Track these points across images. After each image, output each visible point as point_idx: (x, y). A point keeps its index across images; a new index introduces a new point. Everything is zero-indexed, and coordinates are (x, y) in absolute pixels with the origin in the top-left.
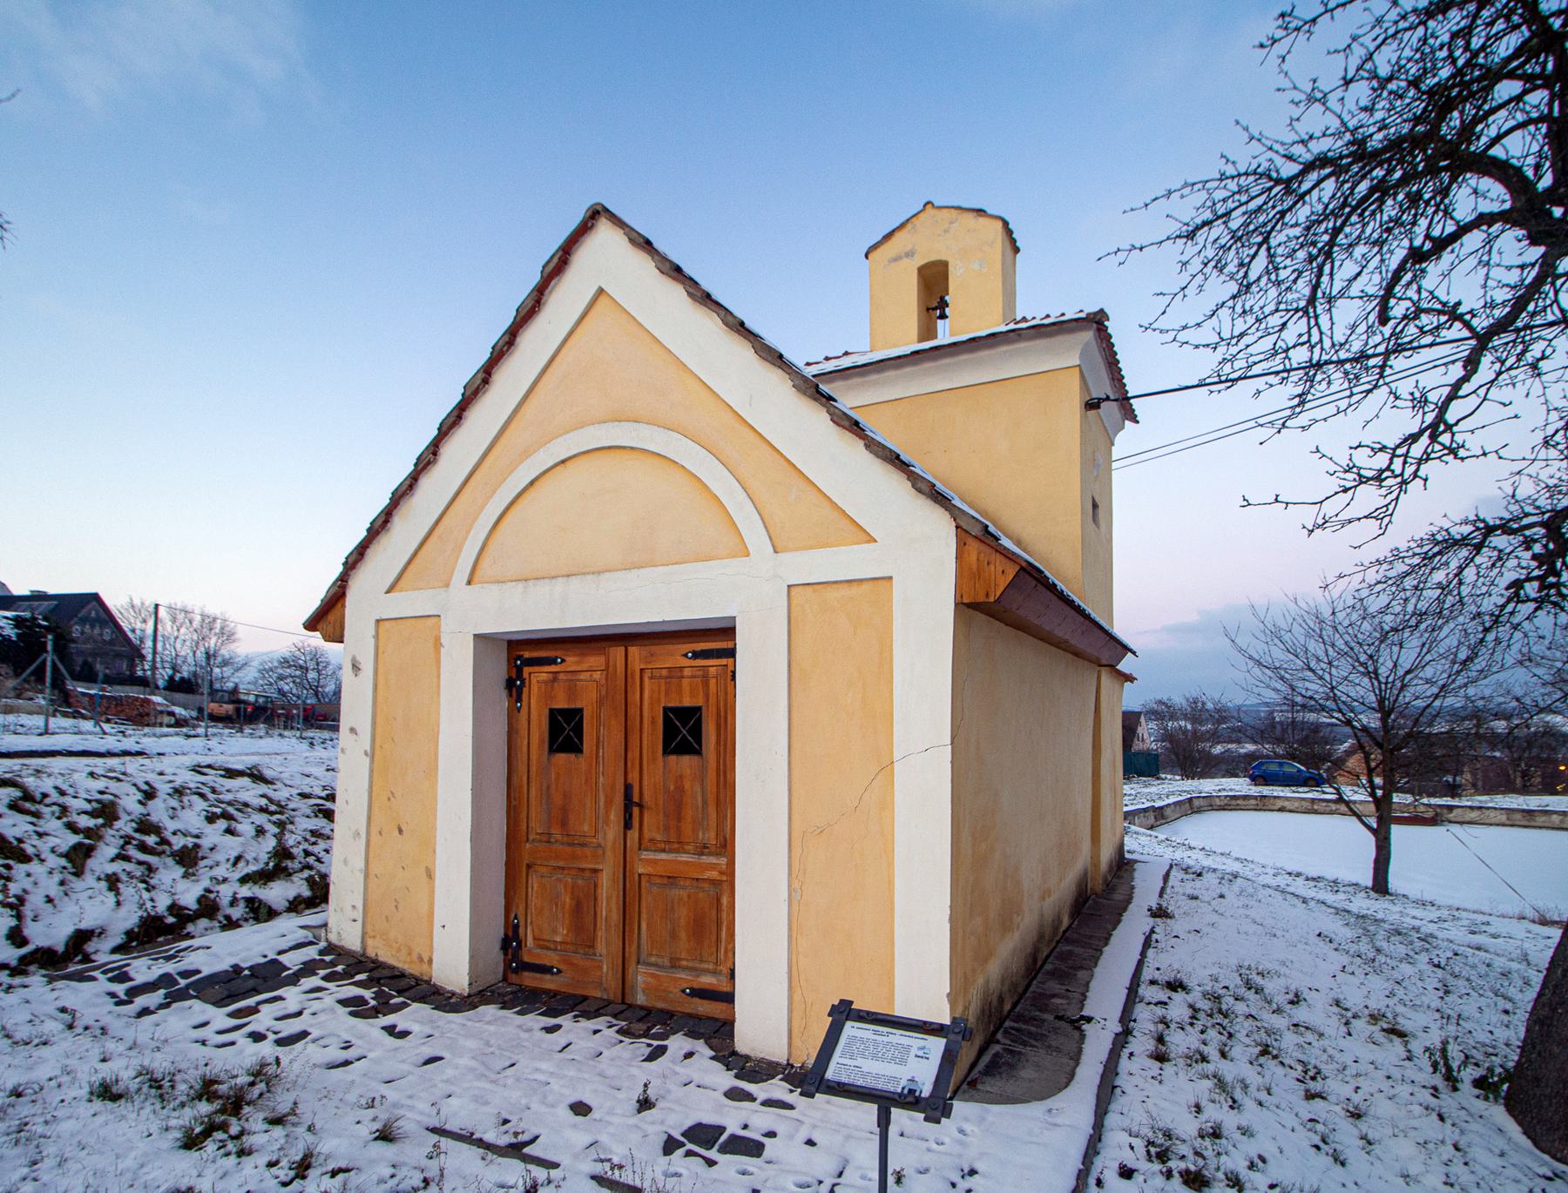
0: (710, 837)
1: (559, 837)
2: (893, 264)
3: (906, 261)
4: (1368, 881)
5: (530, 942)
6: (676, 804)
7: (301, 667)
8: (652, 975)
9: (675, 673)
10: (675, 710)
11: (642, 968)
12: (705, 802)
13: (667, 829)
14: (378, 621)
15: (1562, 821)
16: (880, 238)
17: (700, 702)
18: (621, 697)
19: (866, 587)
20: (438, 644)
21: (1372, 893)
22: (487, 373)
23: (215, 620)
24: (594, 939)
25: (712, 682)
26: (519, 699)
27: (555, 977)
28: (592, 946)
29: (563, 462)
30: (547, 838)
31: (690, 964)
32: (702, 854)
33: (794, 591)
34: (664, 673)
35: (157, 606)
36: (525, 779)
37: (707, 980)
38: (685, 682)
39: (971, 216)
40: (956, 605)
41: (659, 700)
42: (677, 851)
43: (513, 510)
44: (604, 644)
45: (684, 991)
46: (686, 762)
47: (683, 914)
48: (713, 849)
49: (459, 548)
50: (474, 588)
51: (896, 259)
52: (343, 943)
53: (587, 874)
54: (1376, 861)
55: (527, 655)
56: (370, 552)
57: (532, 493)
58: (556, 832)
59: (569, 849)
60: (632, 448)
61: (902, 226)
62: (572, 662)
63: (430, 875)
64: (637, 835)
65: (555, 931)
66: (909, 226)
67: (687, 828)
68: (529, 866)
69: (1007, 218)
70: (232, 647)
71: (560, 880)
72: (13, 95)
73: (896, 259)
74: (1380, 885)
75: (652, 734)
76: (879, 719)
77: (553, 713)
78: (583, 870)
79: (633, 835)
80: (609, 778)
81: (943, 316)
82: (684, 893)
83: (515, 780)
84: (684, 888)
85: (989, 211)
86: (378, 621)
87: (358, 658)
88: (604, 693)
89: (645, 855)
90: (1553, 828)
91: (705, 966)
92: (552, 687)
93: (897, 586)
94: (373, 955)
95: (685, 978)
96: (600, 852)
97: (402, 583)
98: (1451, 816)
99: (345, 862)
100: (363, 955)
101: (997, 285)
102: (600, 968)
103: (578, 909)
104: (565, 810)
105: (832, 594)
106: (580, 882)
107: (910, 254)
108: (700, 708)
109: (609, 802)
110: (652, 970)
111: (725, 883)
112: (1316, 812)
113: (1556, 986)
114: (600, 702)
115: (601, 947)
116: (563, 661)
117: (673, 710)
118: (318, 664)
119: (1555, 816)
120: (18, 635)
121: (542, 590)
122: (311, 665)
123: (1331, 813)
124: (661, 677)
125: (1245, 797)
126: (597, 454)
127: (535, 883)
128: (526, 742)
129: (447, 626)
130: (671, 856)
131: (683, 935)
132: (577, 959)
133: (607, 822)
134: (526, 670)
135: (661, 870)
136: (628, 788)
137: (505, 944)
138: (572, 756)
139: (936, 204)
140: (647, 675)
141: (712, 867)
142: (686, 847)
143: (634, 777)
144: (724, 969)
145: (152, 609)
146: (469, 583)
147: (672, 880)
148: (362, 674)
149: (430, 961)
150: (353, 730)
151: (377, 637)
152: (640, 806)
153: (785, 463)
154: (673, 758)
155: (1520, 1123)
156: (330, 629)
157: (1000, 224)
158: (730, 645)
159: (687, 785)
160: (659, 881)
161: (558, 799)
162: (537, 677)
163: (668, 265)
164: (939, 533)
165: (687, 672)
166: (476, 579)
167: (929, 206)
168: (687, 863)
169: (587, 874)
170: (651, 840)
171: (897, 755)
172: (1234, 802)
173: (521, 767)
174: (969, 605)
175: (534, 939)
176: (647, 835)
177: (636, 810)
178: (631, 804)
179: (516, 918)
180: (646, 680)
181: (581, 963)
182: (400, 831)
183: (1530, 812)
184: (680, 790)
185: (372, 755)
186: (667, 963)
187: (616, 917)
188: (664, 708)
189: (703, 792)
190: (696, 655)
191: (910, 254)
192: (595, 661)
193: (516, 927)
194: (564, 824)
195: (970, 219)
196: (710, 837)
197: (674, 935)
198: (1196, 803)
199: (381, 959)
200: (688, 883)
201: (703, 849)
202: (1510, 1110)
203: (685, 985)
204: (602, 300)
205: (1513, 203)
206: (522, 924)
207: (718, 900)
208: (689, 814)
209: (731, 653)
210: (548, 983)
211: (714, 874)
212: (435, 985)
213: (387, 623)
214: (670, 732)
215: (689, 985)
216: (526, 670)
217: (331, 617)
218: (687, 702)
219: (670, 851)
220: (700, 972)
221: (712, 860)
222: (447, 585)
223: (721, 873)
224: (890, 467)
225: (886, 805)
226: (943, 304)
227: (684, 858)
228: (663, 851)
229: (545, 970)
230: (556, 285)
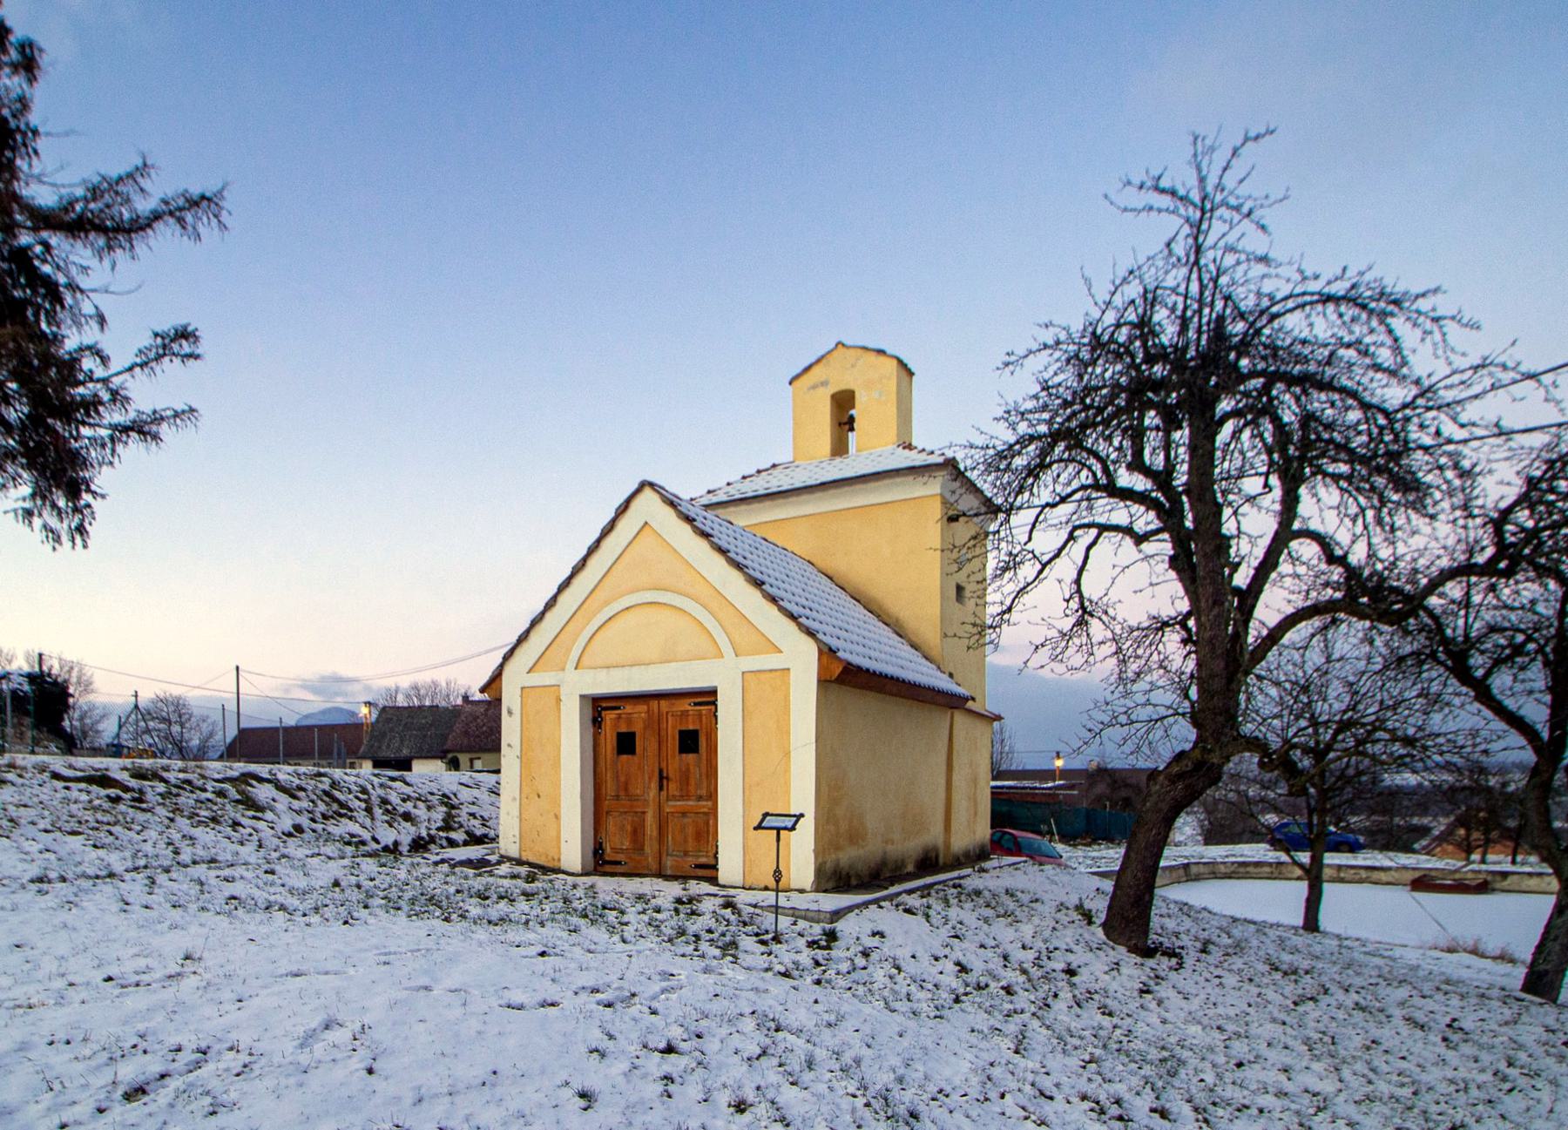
0: (704, 792)
3: (821, 390)
4: (1299, 920)
5: (608, 850)
6: (685, 777)
7: (164, 719)
9: (685, 714)
17: (698, 727)
18: (656, 727)
19: (778, 673)
20: (559, 700)
21: (1301, 931)
22: (584, 561)
23: (72, 668)
24: (643, 845)
30: (617, 797)
33: (746, 675)
35: (40, 655)
37: (703, 860)
40: (819, 681)
43: (601, 632)
46: (691, 757)
47: (690, 830)
49: (569, 650)
51: (814, 387)
54: (1308, 900)
55: (604, 705)
57: (610, 623)
58: (622, 793)
61: (818, 361)
62: (629, 709)
63: (557, 817)
66: (824, 361)
67: (692, 788)
70: (91, 697)
72: (140, 287)
73: (814, 387)
74: (1311, 923)
75: (673, 743)
76: (784, 731)
79: (664, 793)
80: (651, 765)
81: (852, 429)
82: (690, 820)
83: (599, 770)
89: (671, 803)
93: (792, 673)
95: (691, 860)
98: (1506, 884)
101: (892, 410)
103: (635, 832)
104: (626, 784)
105: (762, 676)
107: (824, 384)
109: (650, 778)
111: (713, 812)
112: (1342, 881)
114: (645, 728)
115: (647, 849)
118: (180, 717)
120: (33, 691)
122: (174, 718)
123: (1361, 881)
125: (1258, 864)
127: (611, 820)
129: (563, 691)
133: (649, 788)
134: (603, 713)
136: (661, 771)
137: (595, 852)
143: (664, 765)
144: (711, 854)
145: (36, 659)
147: (684, 814)
149: (559, 860)
150: (509, 745)
152: (667, 778)
157: (895, 362)
158: (712, 699)
161: (622, 779)
162: (609, 716)
164: (810, 650)
172: (1242, 870)
173: (602, 764)
174: (826, 681)
176: (671, 793)
177: (665, 782)
178: (662, 778)
184: (688, 770)
185: (520, 757)
187: (655, 833)
190: (696, 704)
191: (824, 384)
193: (601, 844)
194: (626, 790)
195: (872, 357)
196: (704, 792)
197: (686, 841)
198: (1194, 870)
201: (700, 798)
204: (647, 529)
208: (692, 782)
209: (714, 703)
211: (706, 810)
216: (603, 713)
217: (494, 686)
220: (699, 857)
221: (704, 803)
222: (563, 669)
225: (787, 770)
226: (852, 420)
227: (691, 803)
229: (618, 863)
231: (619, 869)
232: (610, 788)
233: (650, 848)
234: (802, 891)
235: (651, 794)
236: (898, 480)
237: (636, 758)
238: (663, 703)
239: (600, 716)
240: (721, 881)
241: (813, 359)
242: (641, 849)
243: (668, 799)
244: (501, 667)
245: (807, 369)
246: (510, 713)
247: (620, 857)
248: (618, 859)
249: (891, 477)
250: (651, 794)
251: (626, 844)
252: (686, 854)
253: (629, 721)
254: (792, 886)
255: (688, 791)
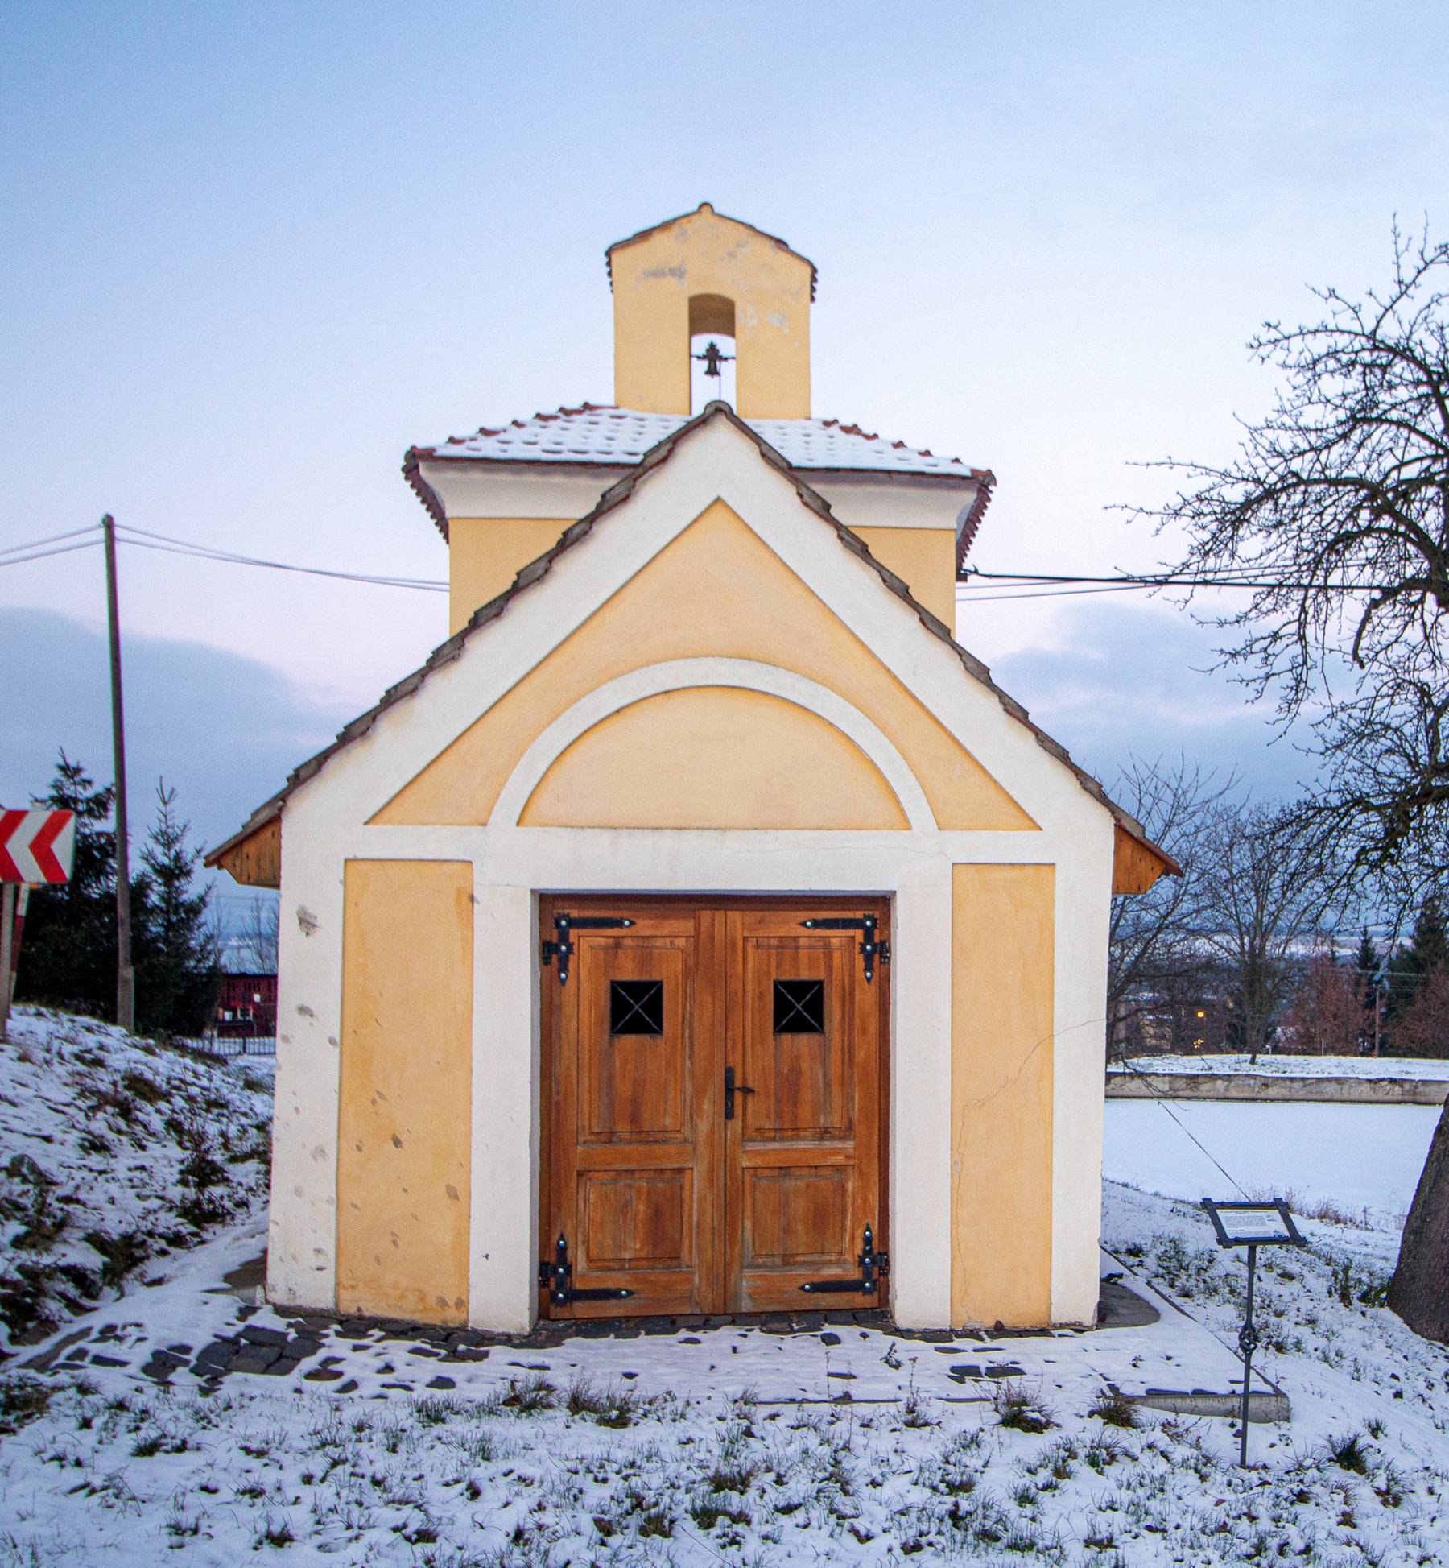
1: (626, 1136)
2: (651, 280)
3: (670, 282)
5: (581, 1264)
6: (790, 1087)
8: (761, 1277)
10: (789, 985)
11: (747, 1272)
12: (827, 1084)
13: (779, 1115)
14: (347, 861)
15: (1227, 1089)
16: (629, 235)
17: (819, 975)
19: (1029, 871)
25: (837, 955)
26: (564, 968)
27: (622, 1302)
28: (678, 1258)
29: (666, 692)
30: (609, 1137)
31: (807, 1259)
32: (822, 1139)
34: (774, 942)
36: (574, 1067)
38: (803, 953)
39: (768, 245)
41: (769, 973)
42: (791, 1139)
44: (691, 906)
45: (802, 1288)
46: (804, 1042)
47: (800, 1207)
48: (837, 1133)
50: (520, 828)
51: (656, 274)
52: (299, 1302)
53: (668, 1175)
55: (574, 914)
56: (332, 764)
59: (641, 1148)
60: (764, 693)
61: (666, 226)
62: (645, 926)
64: (740, 1124)
65: (621, 1247)
66: (676, 230)
67: (805, 1112)
68: (580, 1174)
69: (817, 264)
71: (630, 1186)
73: (656, 274)
77: (616, 986)
78: (662, 1170)
79: (736, 1124)
82: (801, 1184)
84: (798, 1177)
85: (793, 246)
86: (347, 861)
87: (310, 910)
88: (691, 962)
89: (750, 1146)
90: (1217, 1099)
91: (826, 1257)
92: (616, 956)
93: (1060, 874)
94: (353, 1311)
95: (805, 1275)
96: (689, 1147)
97: (386, 815)
99: (298, 1192)
100: (335, 1314)
102: (691, 1280)
103: (657, 1216)
104: (636, 1104)
106: (660, 1185)
108: (821, 983)
110: (761, 1272)
113: (1425, 1202)
114: (689, 973)
116: (632, 923)
117: (785, 984)
119: (1219, 1082)
121: (644, 842)
124: (769, 947)
126: (714, 690)
128: (574, 1023)
130: (786, 1145)
131: (800, 1228)
132: (660, 1276)
134: (573, 934)
135: (772, 1161)
136: (729, 1073)
138: (646, 1039)
139: (717, 210)
140: (752, 943)
141: (836, 1152)
142: (802, 1134)
143: (736, 1061)
146: (518, 824)
147: (784, 1170)
148: (318, 935)
149: (461, 1304)
150: (303, 1010)
151: (344, 882)
153: (950, 742)
154: (787, 1038)
155: (1401, 1316)
156: (251, 866)
157: (808, 271)
159: (805, 1066)
160: (767, 1173)
161: (624, 1090)
162: (587, 944)
163: (820, 503)
164: (1102, 828)
165: (802, 942)
166: (528, 818)
167: (706, 209)
168: (804, 1150)
169: (668, 1175)
170: (758, 1130)
171: (1057, 1028)
175: (590, 1260)
177: (738, 1096)
179: (562, 1237)
180: (750, 949)
181: (663, 1279)
182: (397, 1143)
183: (1192, 1078)
184: (797, 1072)
186: (778, 1261)
188: (777, 983)
189: (825, 1075)
190: (817, 924)
191: (678, 273)
192: (686, 926)
193: (562, 1251)
194: (635, 1118)
195: (767, 249)
197: (788, 1230)
199: (367, 1314)
200: (805, 1171)
201: (824, 1133)
202: (1393, 1309)
203: (804, 1281)
205: (1430, 563)
206: (571, 1244)
207: (843, 1188)
208: (806, 1096)
210: (612, 1309)
211: (839, 1160)
212: (474, 1331)
213: (364, 866)
214: (655, 1008)
215: (810, 1281)
216: (573, 934)
218: (805, 975)
219: (781, 1139)
221: (838, 1144)
223: (848, 1157)
224: (1058, 762)
227: (802, 1145)
228: (773, 1139)
230: (652, 475)
231: (612, 1309)
232: (585, 1112)
233: (697, 1253)
234: (1079, 1328)
235: (703, 1127)
236: (894, 490)
237: (662, 1044)
238: (736, 917)
239: (564, 937)
240: (902, 1319)
241: (656, 222)
242: (673, 1257)
243: (746, 1138)
244: (283, 797)
245: (644, 235)
246: (307, 923)
247: (610, 1281)
248: (610, 1285)
249: (878, 482)
250: (703, 1127)
251: (634, 1247)
252: (788, 1260)
253: (645, 956)
254: (1056, 1318)
255: (795, 1117)
